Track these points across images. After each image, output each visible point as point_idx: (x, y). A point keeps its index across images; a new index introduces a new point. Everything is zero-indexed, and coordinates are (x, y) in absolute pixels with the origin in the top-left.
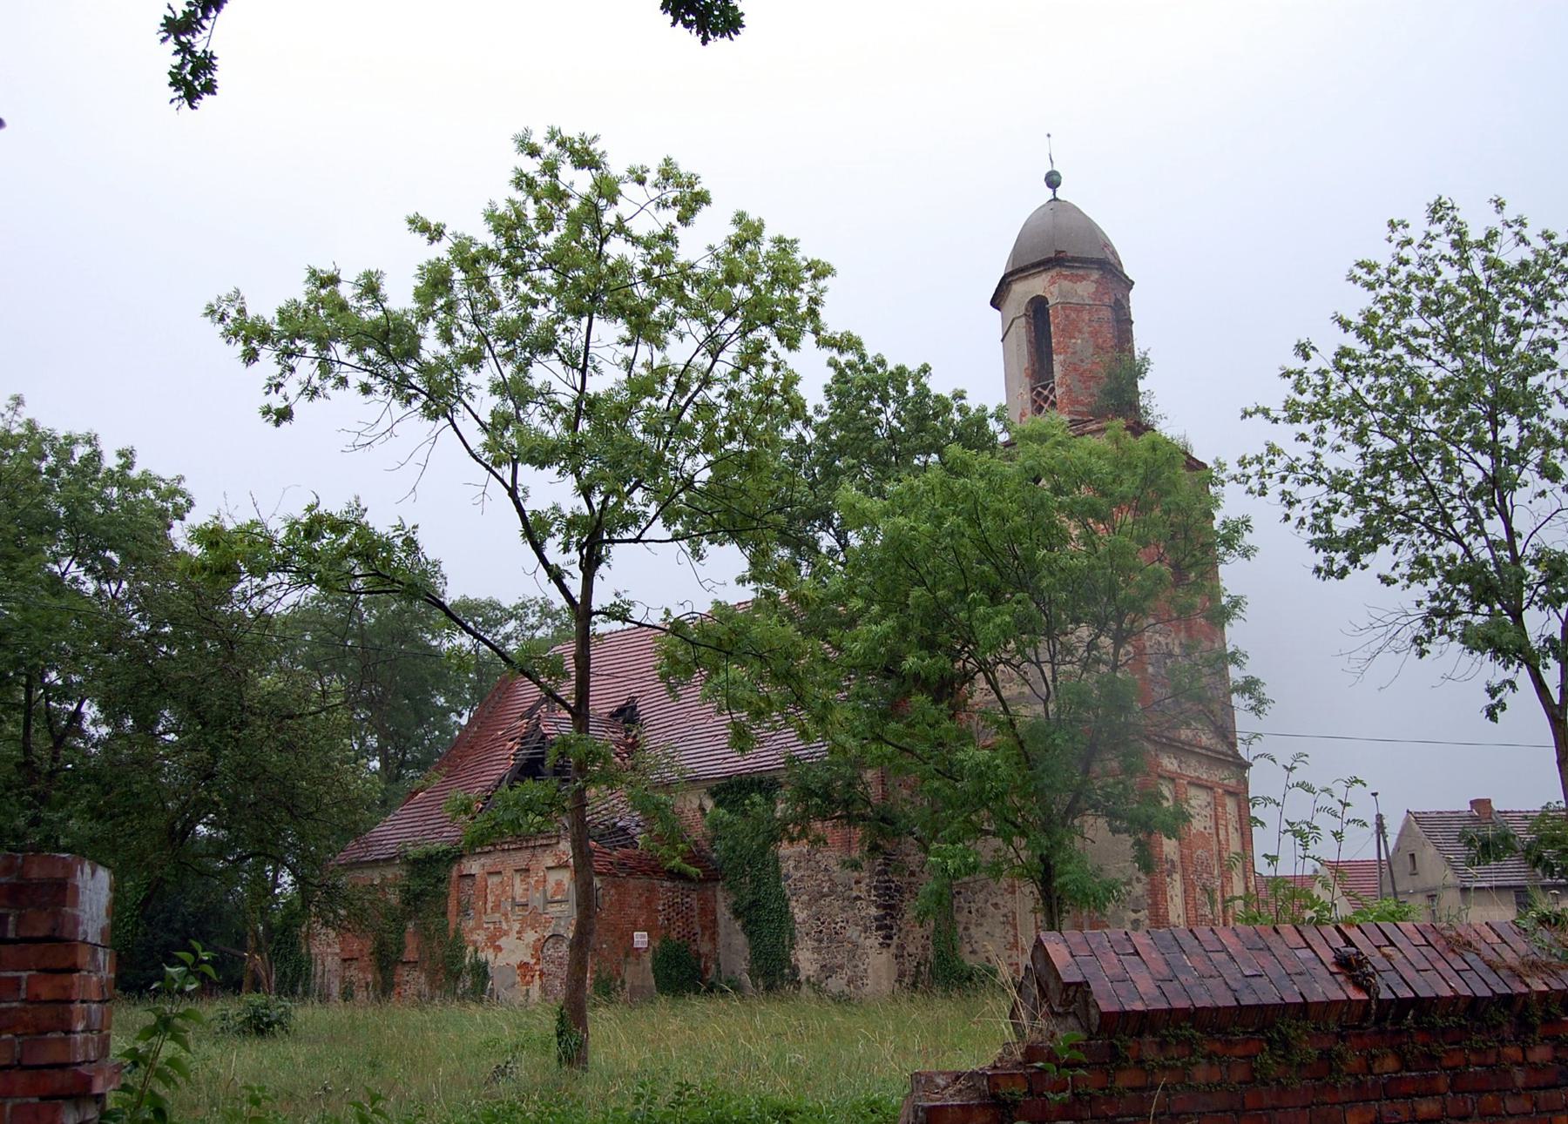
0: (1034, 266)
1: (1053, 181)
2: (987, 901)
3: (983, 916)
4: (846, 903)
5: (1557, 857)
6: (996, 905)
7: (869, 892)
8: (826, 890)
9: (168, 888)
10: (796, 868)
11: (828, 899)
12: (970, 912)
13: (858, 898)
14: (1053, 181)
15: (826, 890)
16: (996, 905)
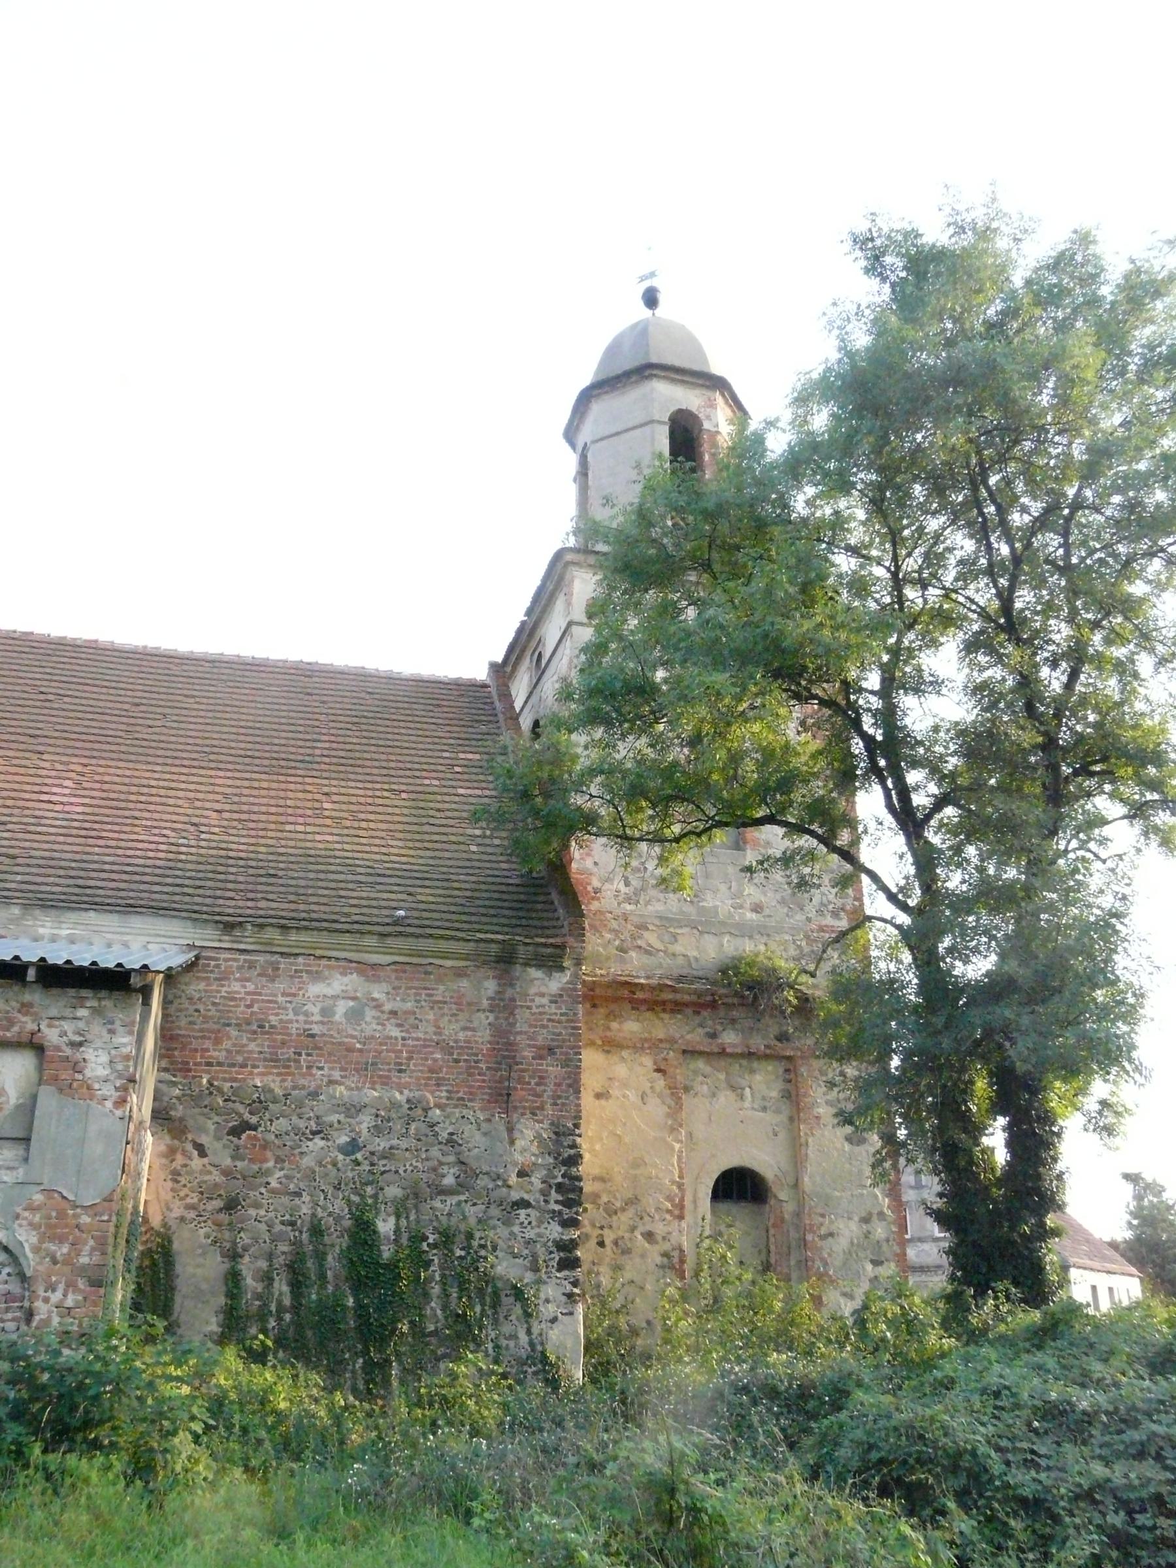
0: (627, 374)
1: (651, 299)
2: (633, 1229)
3: (626, 1252)
4: (495, 1211)
5: (206, 1131)
6: (649, 1236)
7: (545, 1194)
8: (449, 1181)
9: (825, 1047)
10: (377, 1130)
11: (454, 1200)
12: (601, 1244)
13: (523, 1204)
14: (651, 299)
15: (449, 1181)
16: (649, 1236)
